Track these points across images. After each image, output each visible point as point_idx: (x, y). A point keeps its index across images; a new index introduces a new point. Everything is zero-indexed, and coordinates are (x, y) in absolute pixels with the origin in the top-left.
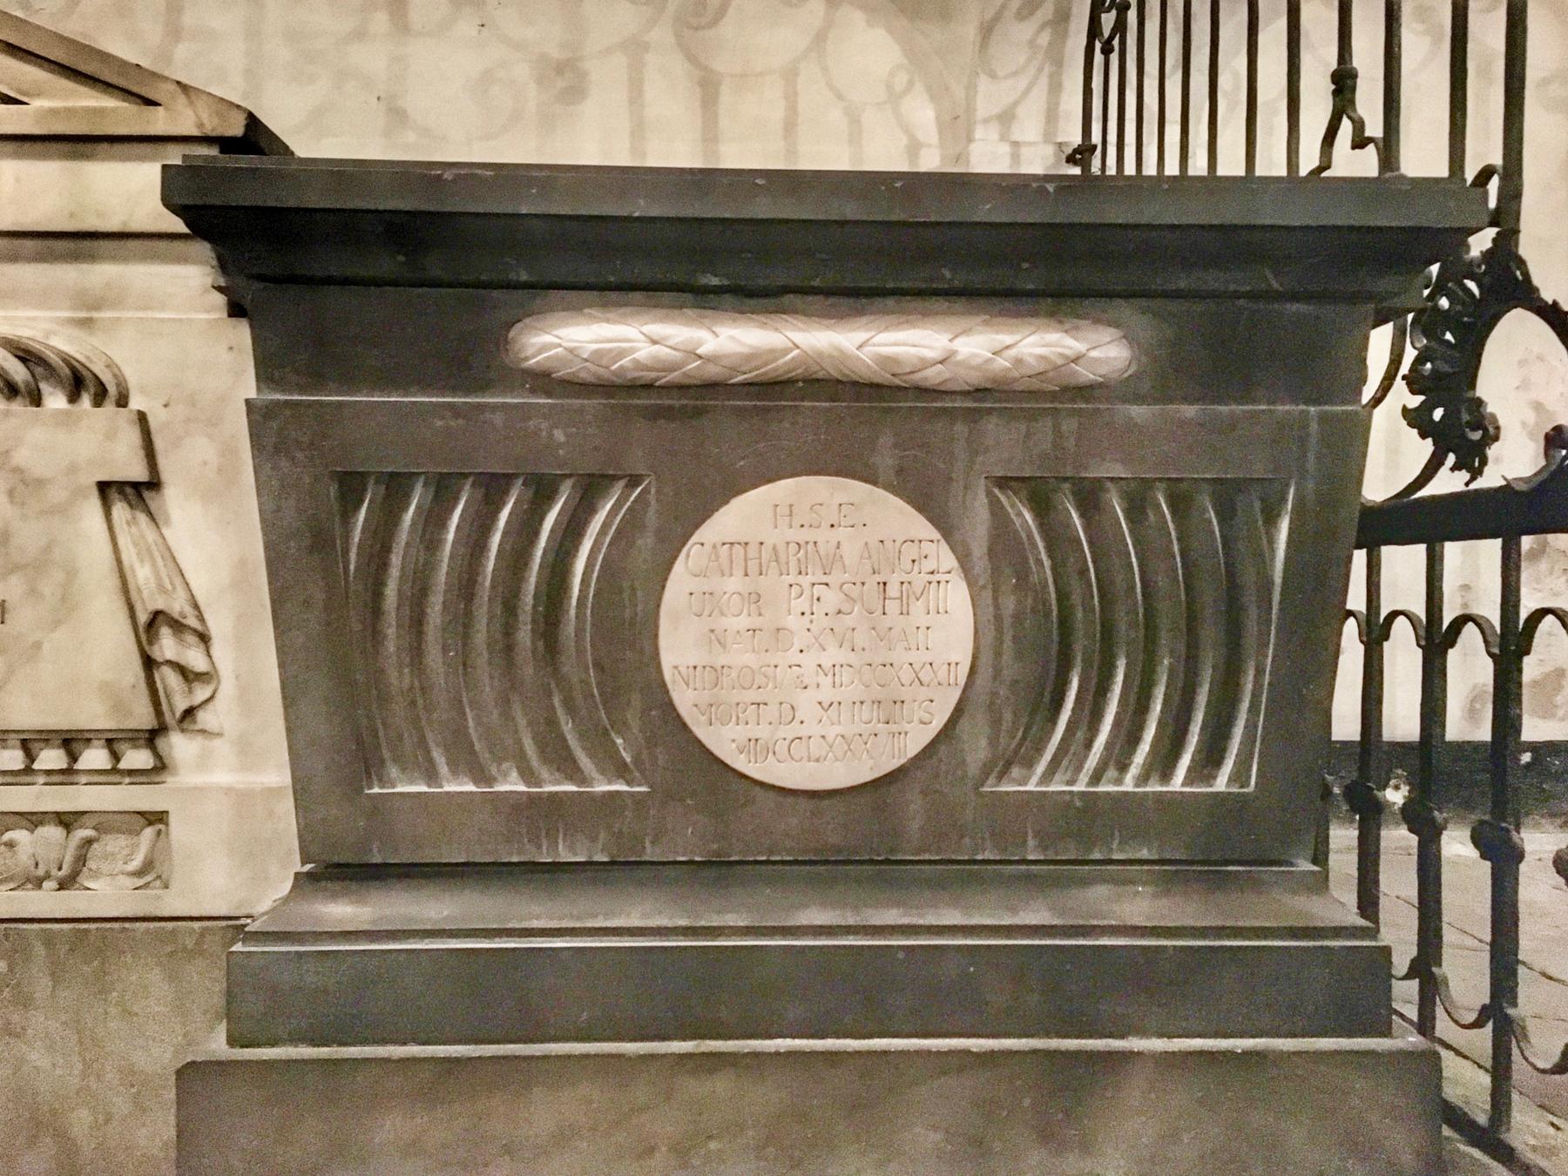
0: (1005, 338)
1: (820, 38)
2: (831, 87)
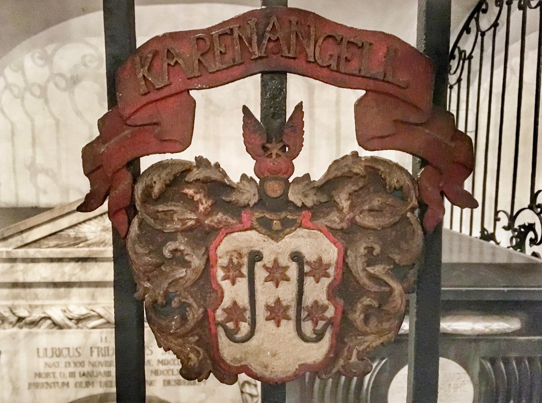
0: (488, 324)
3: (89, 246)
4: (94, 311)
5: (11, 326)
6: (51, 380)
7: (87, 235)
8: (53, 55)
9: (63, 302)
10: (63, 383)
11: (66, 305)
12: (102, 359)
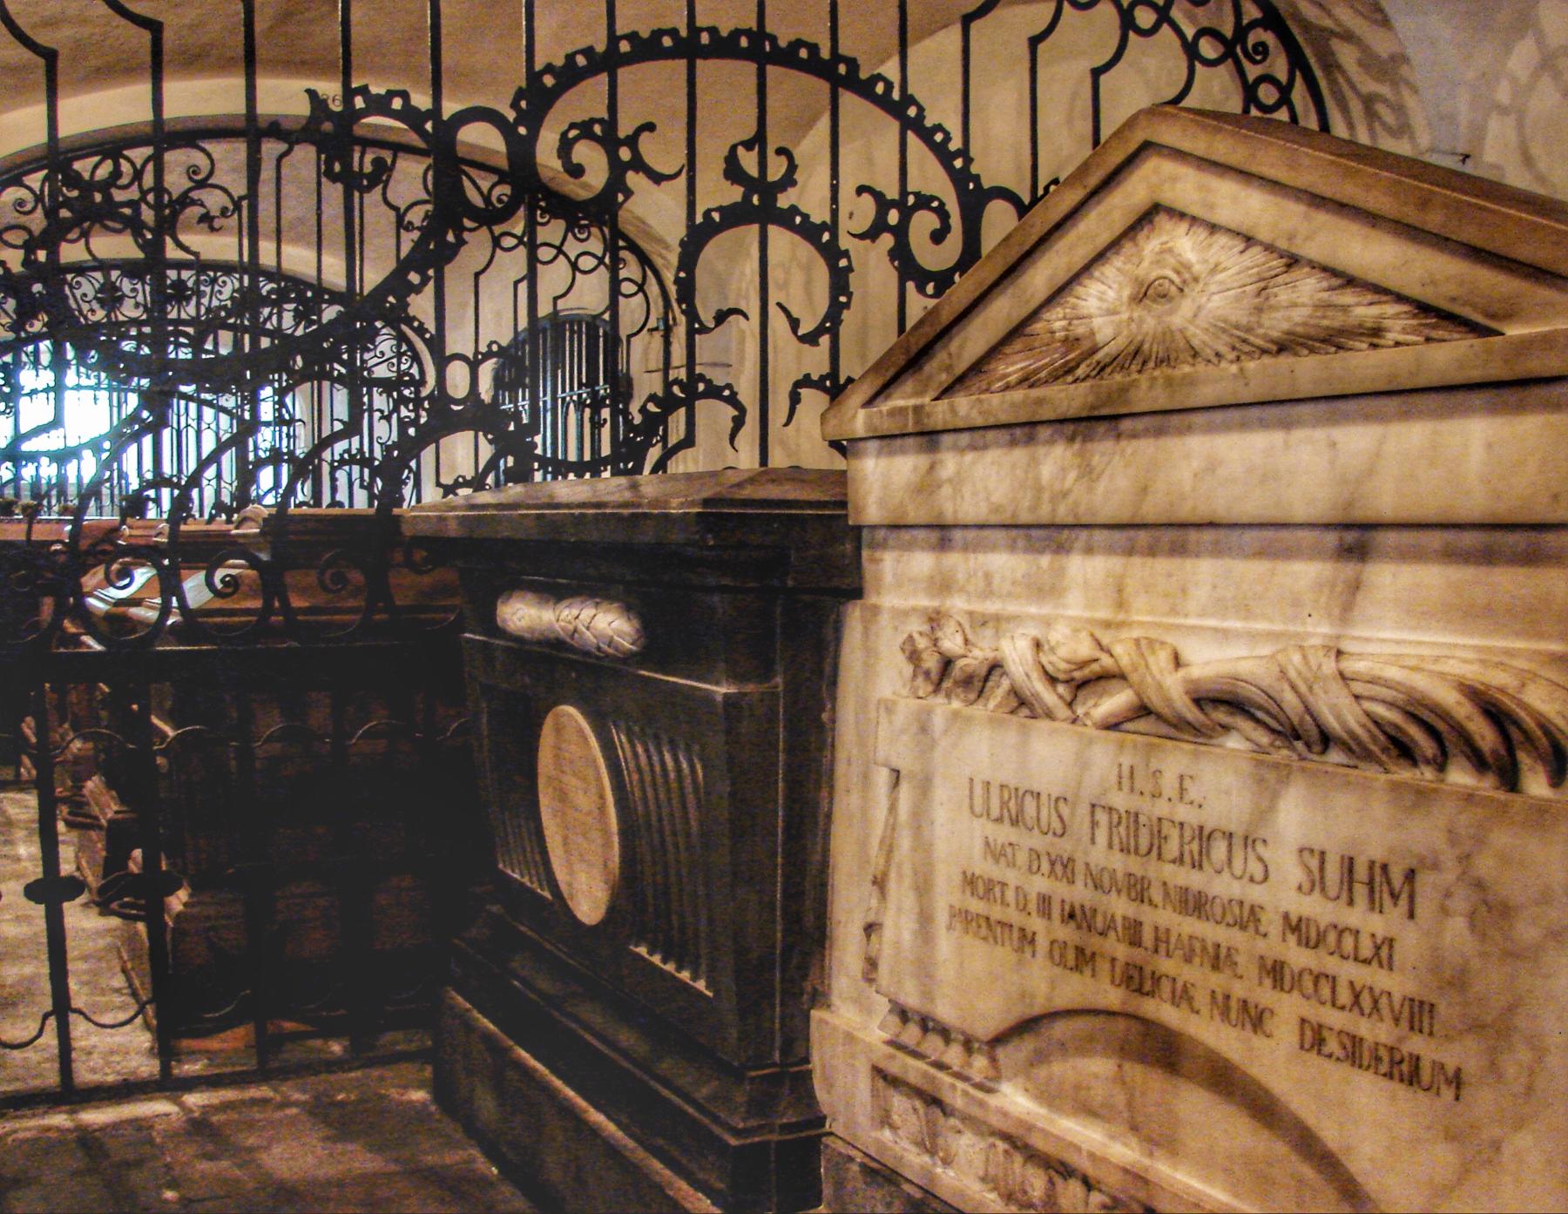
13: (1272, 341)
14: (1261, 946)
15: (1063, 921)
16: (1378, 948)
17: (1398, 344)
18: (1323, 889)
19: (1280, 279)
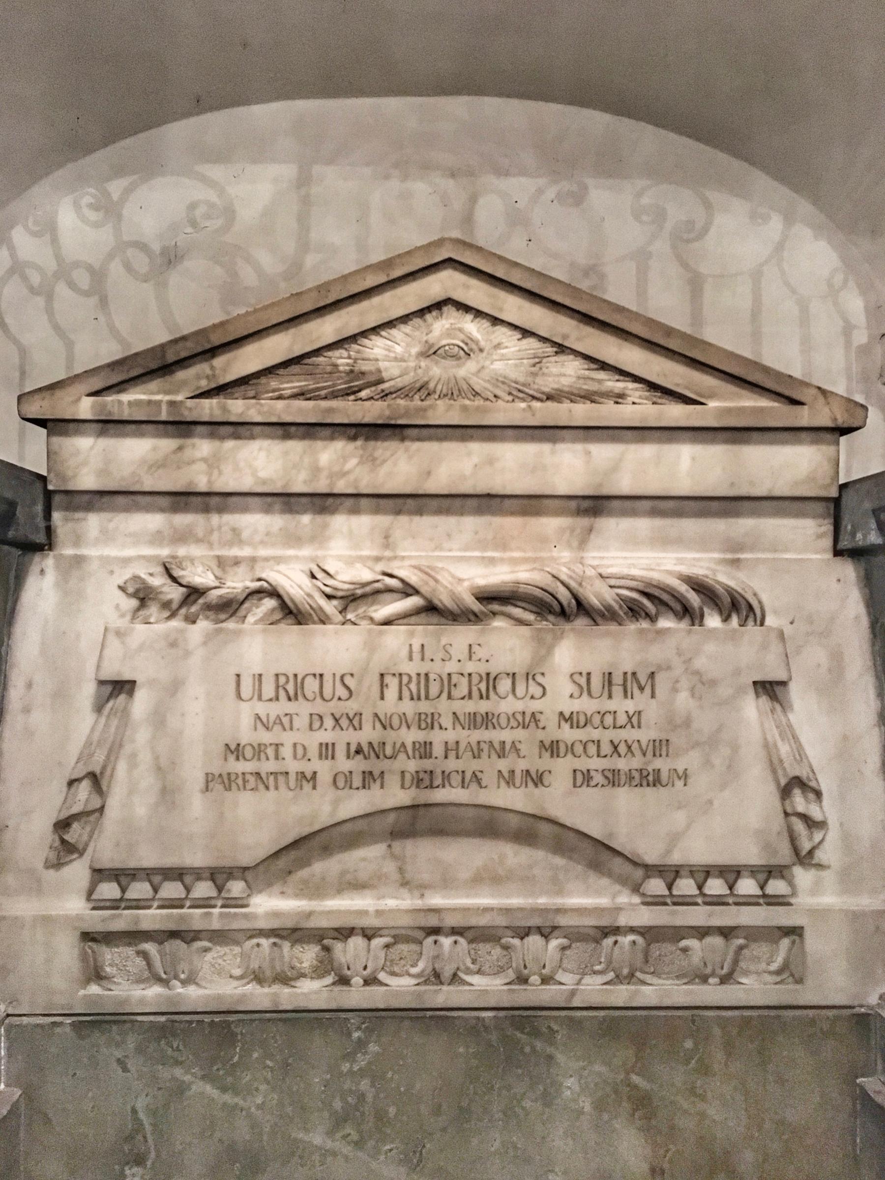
1: (780, 247)
2: (787, 284)
3: (385, 395)
4: (391, 576)
5: (167, 614)
6: (268, 766)
7: (382, 365)
8: (123, 199)
9: (306, 552)
10: (302, 775)
11: (313, 559)
12: (408, 708)
13: (543, 393)
14: (540, 735)
15: (348, 757)
16: (630, 718)
17: (634, 403)
18: (589, 693)
19: (550, 359)
